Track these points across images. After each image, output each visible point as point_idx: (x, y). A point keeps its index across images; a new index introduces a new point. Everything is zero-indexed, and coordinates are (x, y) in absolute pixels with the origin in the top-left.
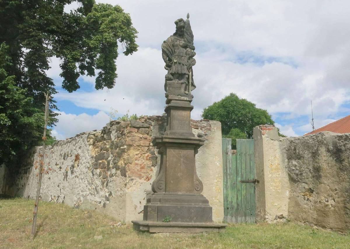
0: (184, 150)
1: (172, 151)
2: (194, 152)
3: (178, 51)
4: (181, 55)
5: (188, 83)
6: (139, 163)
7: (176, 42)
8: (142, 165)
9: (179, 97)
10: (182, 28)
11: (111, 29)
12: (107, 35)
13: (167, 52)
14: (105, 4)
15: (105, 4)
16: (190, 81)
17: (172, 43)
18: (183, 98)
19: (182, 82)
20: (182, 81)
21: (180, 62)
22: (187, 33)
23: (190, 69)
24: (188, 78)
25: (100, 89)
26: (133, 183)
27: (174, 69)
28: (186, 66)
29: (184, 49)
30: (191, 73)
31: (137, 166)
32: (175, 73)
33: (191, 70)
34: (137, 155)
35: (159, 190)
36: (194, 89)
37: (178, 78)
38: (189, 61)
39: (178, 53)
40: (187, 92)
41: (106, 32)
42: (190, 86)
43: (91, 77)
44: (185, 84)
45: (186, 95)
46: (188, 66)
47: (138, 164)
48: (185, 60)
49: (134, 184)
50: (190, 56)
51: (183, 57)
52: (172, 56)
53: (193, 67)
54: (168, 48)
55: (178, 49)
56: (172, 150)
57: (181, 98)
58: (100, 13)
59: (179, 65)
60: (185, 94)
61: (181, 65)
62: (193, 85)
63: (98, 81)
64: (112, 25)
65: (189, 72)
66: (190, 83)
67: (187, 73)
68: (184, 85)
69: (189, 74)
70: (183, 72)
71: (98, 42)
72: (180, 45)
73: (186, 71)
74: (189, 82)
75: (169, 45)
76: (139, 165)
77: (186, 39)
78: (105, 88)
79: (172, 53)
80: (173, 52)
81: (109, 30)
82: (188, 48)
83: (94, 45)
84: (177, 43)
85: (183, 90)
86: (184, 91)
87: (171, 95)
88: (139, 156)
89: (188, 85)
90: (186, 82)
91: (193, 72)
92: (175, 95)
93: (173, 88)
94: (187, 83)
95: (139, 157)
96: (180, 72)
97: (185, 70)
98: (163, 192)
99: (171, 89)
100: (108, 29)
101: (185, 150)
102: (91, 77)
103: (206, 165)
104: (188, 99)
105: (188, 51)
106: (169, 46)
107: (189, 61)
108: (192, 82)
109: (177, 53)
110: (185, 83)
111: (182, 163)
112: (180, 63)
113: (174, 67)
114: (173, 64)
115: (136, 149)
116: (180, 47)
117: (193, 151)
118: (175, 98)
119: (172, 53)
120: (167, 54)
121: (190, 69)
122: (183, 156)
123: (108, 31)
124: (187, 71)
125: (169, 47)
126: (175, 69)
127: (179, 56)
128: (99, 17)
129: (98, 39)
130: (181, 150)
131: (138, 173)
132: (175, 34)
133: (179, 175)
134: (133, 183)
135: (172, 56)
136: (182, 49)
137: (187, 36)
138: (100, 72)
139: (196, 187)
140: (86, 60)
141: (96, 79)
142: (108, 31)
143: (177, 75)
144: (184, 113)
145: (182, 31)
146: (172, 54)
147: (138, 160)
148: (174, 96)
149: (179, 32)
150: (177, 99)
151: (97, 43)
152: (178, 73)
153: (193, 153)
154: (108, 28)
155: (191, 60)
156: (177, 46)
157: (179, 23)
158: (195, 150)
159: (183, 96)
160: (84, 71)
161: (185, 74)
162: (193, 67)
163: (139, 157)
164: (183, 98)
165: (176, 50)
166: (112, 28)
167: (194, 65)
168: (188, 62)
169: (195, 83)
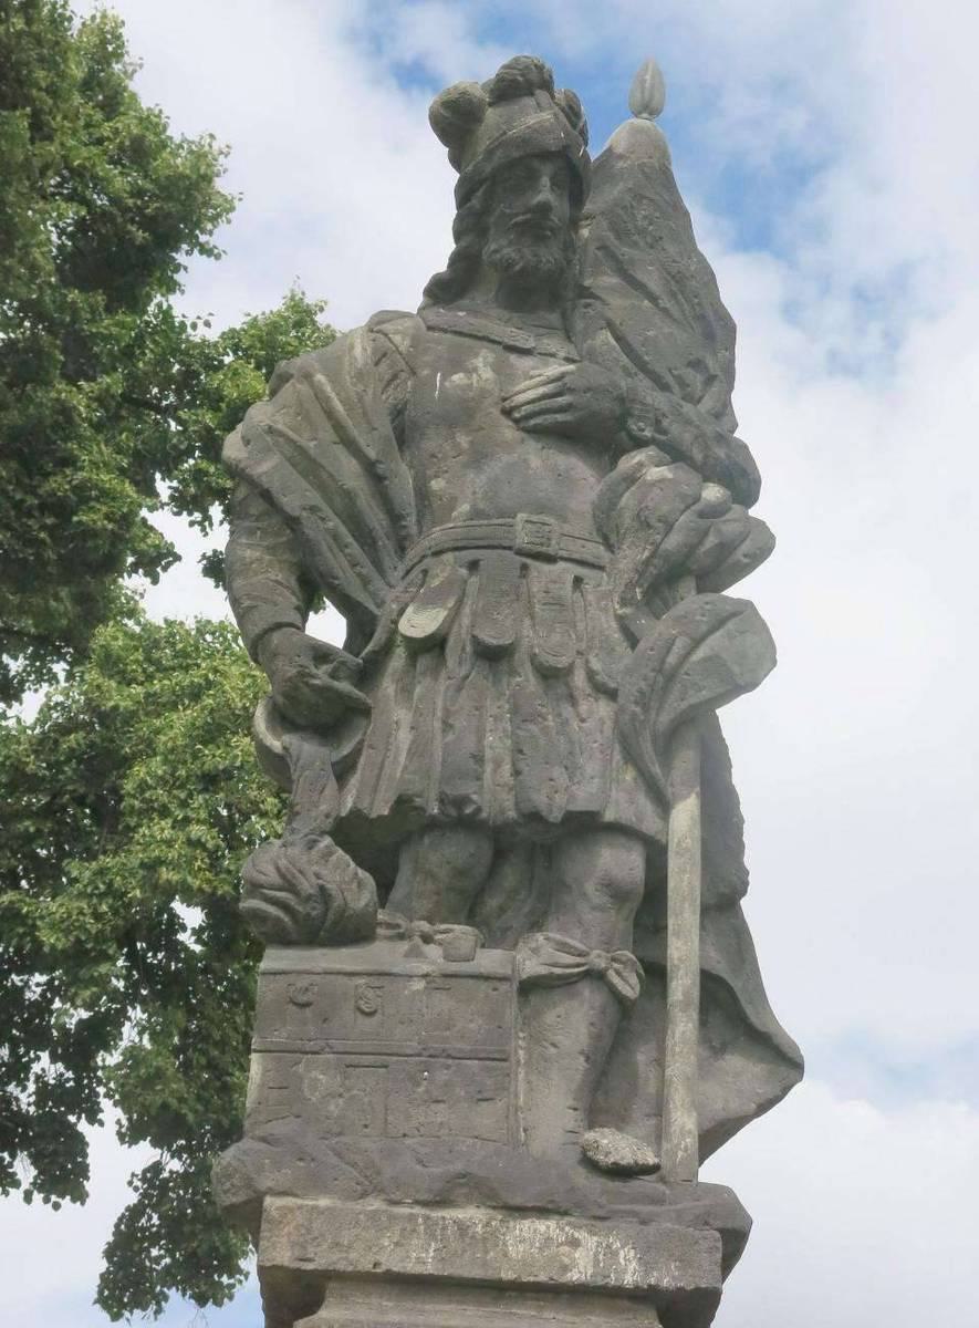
3: (476, 482)
4: (523, 538)
5: (644, 993)
7: (456, 364)
9: (462, 1228)
10: (532, 178)
11: (205, 790)
12: (167, 834)
13: (291, 503)
14: (191, 624)
15: (191, 624)
16: (685, 948)
17: (391, 397)
18: (527, 1245)
19: (532, 967)
20: (536, 956)
21: (490, 637)
22: (623, 271)
23: (676, 735)
24: (647, 909)
25: (137, 1312)
27: (404, 737)
28: (604, 709)
29: (577, 466)
30: (685, 816)
32: (402, 803)
33: (686, 760)
36: (764, 1107)
37: (468, 902)
38: (654, 631)
39: (476, 514)
40: (618, 1146)
41: (164, 812)
42: (683, 1026)
43: (56, 1206)
44: (589, 995)
45: (600, 1183)
46: (629, 689)
48: (584, 618)
50: (673, 542)
51: (551, 559)
52: (377, 564)
53: (732, 718)
54: (320, 441)
55: (478, 458)
57: (490, 1239)
58: (136, 690)
59: (478, 676)
60: (582, 1178)
61: (528, 680)
62: (735, 1016)
63: (126, 1246)
64: (214, 758)
65: (664, 805)
66: (683, 985)
67: (623, 802)
68: (574, 1024)
69: (651, 825)
70: (558, 796)
71: (104, 908)
72: (507, 413)
73: (594, 781)
74: (656, 974)
75: (339, 407)
77: (606, 337)
78: (178, 1303)
79: (376, 519)
80: (395, 518)
81: (190, 796)
82: (640, 443)
83: (67, 932)
84: (458, 378)
85: (548, 1112)
86: (571, 1119)
87: (316, 1184)
89: (629, 1024)
90: (598, 959)
91: (740, 778)
92: (379, 1190)
93: (350, 1061)
94: (629, 986)
96: (494, 796)
97: (591, 767)
99: (319, 1078)
100: (183, 796)
102: (56, 1206)
104: (629, 1271)
105: (631, 479)
106: (338, 427)
107: (643, 622)
108: (709, 981)
109: (465, 508)
110: (596, 976)
112: (493, 657)
113: (402, 715)
114: (388, 686)
116: (509, 432)
118: (393, 1262)
119: (376, 519)
120: (292, 522)
121: (668, 742)
123: (184, 804)
124: (629, 775)
125: (328, 434)
126: (418, 750)
127: (473, 549)
128: (134, 714)
129: (110, 885)
132: (442, 291)
135: (377, 564)
136: (538, 458)
137: (616, 302)
138: (156, 1168)
140: (36, 1068)
141: (117, 1226)
142: (184, 804)
143: (445, 855)
145: (535, 226)
146: (386, 545)
148: (375, 1204)
149: (499, 247)
150: (422, 1258)
151: (98, 916)
152: (460, 819)
154: (182, 787)
155: (690, 601)
156: (461, 413)
157: (492, 115)
159: (542, 1212)
160: (13, 1156)
161: (586, 826)
162: (725, 714)
164: (527, 1245)
165: (436, 485)
166: (210, 781)
167: (737, 686)
168: (633, 641)
169: (791, 997)
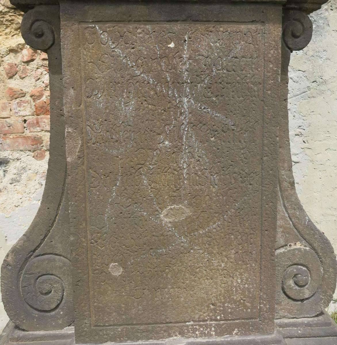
0: (201, 27)
1: (104, 37)
2: (284, 34)
6: (25, 90)
8: (41, 96)
26: (10, 176)
31: (19, 105)
34: (12, 51)
35: (36, 313)
47: (24, 95)
49: (13, 181)
56: (103, 34)
76: (28, 98)
88: (25, 59)
95: (28, 62)
98: (62, 327)
101: (211, 26)
103: (325, 82)
111: (186, 130)
115: (7, 27)
117: (275, 31)
122: (196, 75)
130: (177, 27)
131: (27, 133)
133: (166, 218)
134: (10, 176)
139: (291, 282)
144: (289, 51)
147: (20, 73)
153: (275, 53)
158: (286, 20)
163: (28, 62)
